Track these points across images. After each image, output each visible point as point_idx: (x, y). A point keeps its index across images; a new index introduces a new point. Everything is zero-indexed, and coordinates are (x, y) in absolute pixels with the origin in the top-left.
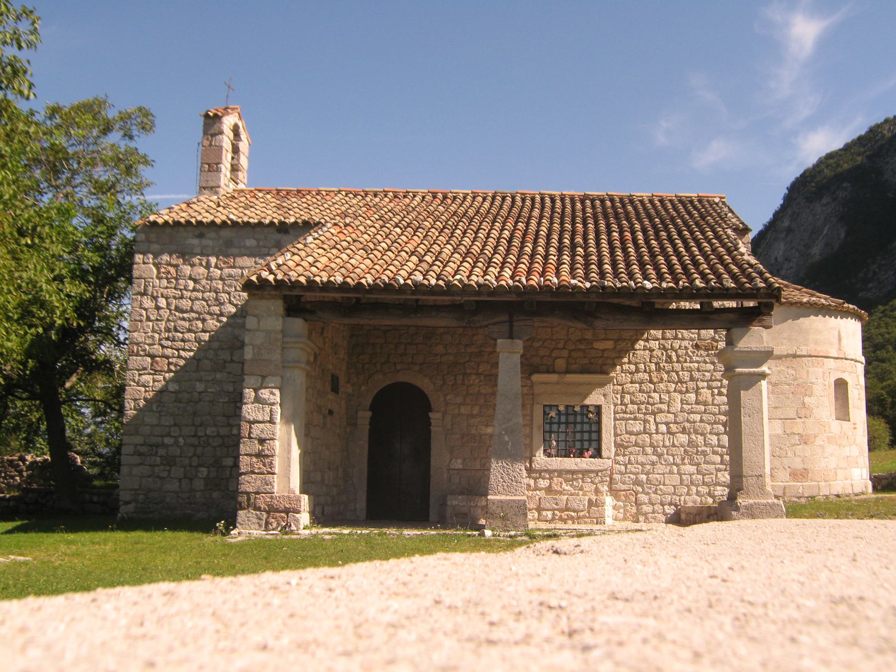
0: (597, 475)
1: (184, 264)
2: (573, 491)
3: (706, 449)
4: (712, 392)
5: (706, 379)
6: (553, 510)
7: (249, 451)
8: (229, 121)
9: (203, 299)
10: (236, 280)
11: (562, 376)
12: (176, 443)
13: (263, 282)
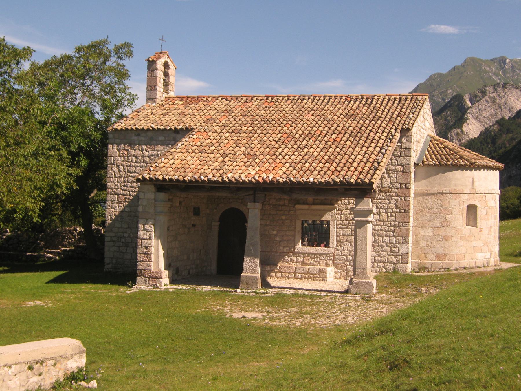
0: (327, 256)
1: (131, 149)
2: (315, 263)
3: (383, 244)
4: (388, 215)
5: (384, 208)
6: (302, 273)
7: (141, 252)
8: (160, 63)
9: (140, 166)
10: (155, 157)
11: (310, 205)
12: (129, 236)
13: (144, 179)
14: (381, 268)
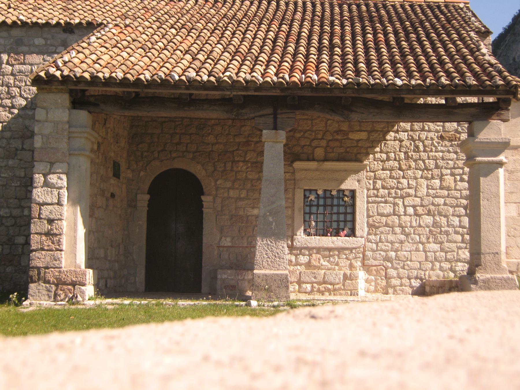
0: (352, 252)
2: (330, 266)
3: (448, 229)
4: (455, 178)
5: (449, 167)
6: (312, 283)
7: (39, 230)
10: (26, 76)
11: (321, 163)
13: (51, 78)
14: (446, 271)
